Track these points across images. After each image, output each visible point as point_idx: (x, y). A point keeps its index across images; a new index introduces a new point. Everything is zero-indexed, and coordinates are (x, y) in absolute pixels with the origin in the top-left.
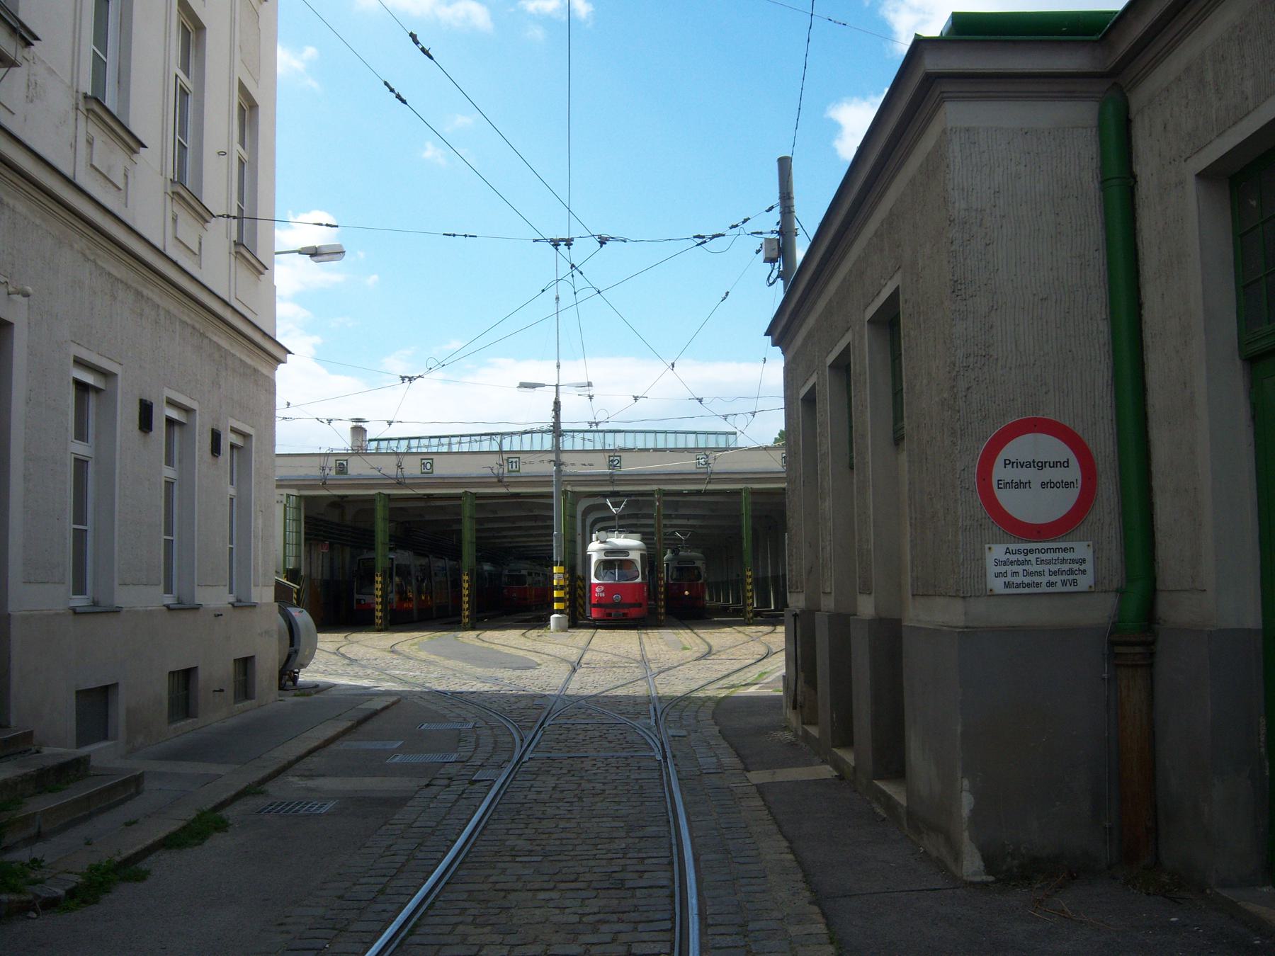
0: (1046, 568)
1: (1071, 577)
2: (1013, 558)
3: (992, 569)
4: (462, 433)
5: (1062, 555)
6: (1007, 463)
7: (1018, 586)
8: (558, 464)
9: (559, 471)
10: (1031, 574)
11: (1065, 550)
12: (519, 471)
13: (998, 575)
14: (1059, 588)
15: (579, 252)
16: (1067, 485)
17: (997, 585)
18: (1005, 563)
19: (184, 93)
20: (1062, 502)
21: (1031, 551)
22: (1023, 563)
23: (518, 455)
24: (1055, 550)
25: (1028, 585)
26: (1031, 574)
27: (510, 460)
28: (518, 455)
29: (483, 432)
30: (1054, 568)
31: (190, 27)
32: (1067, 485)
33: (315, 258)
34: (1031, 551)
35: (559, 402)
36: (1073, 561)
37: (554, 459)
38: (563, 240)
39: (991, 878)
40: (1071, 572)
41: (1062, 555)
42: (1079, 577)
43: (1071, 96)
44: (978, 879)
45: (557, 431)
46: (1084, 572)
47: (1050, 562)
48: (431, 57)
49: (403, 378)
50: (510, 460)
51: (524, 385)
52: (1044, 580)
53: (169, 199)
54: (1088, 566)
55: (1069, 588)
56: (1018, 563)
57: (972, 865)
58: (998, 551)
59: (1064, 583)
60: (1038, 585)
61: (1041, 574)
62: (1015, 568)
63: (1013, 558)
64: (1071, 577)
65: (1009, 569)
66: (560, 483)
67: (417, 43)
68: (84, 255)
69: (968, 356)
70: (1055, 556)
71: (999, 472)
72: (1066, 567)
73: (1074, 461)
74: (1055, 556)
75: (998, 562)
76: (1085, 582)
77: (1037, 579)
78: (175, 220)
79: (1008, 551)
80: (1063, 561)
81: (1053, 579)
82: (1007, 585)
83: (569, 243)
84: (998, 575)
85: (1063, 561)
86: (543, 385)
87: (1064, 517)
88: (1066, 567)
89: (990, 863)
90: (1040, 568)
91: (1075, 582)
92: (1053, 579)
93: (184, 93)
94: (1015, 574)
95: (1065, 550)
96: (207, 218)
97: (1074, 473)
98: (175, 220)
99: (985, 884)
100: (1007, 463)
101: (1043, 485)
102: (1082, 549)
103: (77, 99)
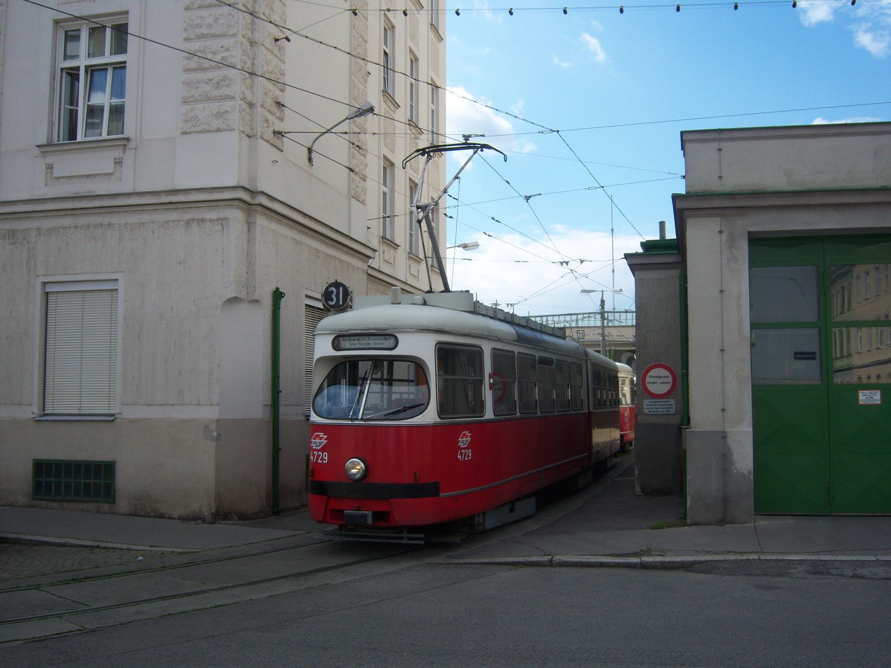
0: (661, 407)
1: (668, 409)
2: (651, 404)
3: (645, 407)
4: (553, 314)
5: (666, 403)
6: (650, 376)
7: (652, 412)
8: (603, 335)
9: (604, 340)
10: (656, 408)
11: (667, 402)
12: (584, 338)
13: (647, 409)
14: (665, 413)
15: (572, 265)
16: (668, 383)
17: (646, 411)
18: (649, 405)
19: (386, 54)
20: (666, 388)
21: (657, 402)
22: (655, 405)
23: (583, 329)
24: (664, 402)
25: (656, 412)
26: (656, 408)
27: (579, 332)
28: (583, 329)
29: (567, 313)
30: (663, 407)
31: (413, 185)
32: (668, 383)
33: (466, 248)
34: (657, 402)
35: (604, 301)
36: (670, 405)
37: (601, 332)
38: (564, 262)
39: (643, 494)
40: (668, 408)
41: (666, 403)
42: (671, 410)
43: (673, 268)
44: (640, 494)
45: (602, 313)
46: (672, 408)
47: (663, 405)
48: (500, 222)
49: (508, 305)
50: (579, 332)
51: (584, 291)
52: (661, 410)
53: (407, 260)
54: (674, 407)
55: (667, 413)
56: (653, 405)
57: (638, 490)
58: (647, 402)
59: (666, 411)
60: (659, 412)
61: (659, 408)
62: (652, 407)
63: (651, 404)
64: (668, 409)
65: (650, 407)
66: (605, 346)
67: (494, 220)
68: (383, 292)
69: (639, 346)
70: (664, 403)
71: (648, 379)
72: (667, 407)
73: (670, 376)
74: (664, 403)
75: (647, 405)
76: (673, 411)
77: (658, 410)
78: (410, 267)
79: (650, 402)
80: (666, 405)
81: (663, 410)
82: (650, 411)
83: (567, 263)
84: (647, 409)
85: (666, 405)
86: (594, 291)
87: (653, 393)
88: (667, 407)
89: (643, 490)
90: (659, 407)
91: (669, 411)
92: (663, 410)
93: (386, 54)
94: (652, 408)
95: (667, 402)
96: (421, 261)
97: (670, 379)
98: (410, 267)
99: (641, 496)
100: (650, 376)
101: (661, 383)
102: (672, 401)
103: (380, 239)
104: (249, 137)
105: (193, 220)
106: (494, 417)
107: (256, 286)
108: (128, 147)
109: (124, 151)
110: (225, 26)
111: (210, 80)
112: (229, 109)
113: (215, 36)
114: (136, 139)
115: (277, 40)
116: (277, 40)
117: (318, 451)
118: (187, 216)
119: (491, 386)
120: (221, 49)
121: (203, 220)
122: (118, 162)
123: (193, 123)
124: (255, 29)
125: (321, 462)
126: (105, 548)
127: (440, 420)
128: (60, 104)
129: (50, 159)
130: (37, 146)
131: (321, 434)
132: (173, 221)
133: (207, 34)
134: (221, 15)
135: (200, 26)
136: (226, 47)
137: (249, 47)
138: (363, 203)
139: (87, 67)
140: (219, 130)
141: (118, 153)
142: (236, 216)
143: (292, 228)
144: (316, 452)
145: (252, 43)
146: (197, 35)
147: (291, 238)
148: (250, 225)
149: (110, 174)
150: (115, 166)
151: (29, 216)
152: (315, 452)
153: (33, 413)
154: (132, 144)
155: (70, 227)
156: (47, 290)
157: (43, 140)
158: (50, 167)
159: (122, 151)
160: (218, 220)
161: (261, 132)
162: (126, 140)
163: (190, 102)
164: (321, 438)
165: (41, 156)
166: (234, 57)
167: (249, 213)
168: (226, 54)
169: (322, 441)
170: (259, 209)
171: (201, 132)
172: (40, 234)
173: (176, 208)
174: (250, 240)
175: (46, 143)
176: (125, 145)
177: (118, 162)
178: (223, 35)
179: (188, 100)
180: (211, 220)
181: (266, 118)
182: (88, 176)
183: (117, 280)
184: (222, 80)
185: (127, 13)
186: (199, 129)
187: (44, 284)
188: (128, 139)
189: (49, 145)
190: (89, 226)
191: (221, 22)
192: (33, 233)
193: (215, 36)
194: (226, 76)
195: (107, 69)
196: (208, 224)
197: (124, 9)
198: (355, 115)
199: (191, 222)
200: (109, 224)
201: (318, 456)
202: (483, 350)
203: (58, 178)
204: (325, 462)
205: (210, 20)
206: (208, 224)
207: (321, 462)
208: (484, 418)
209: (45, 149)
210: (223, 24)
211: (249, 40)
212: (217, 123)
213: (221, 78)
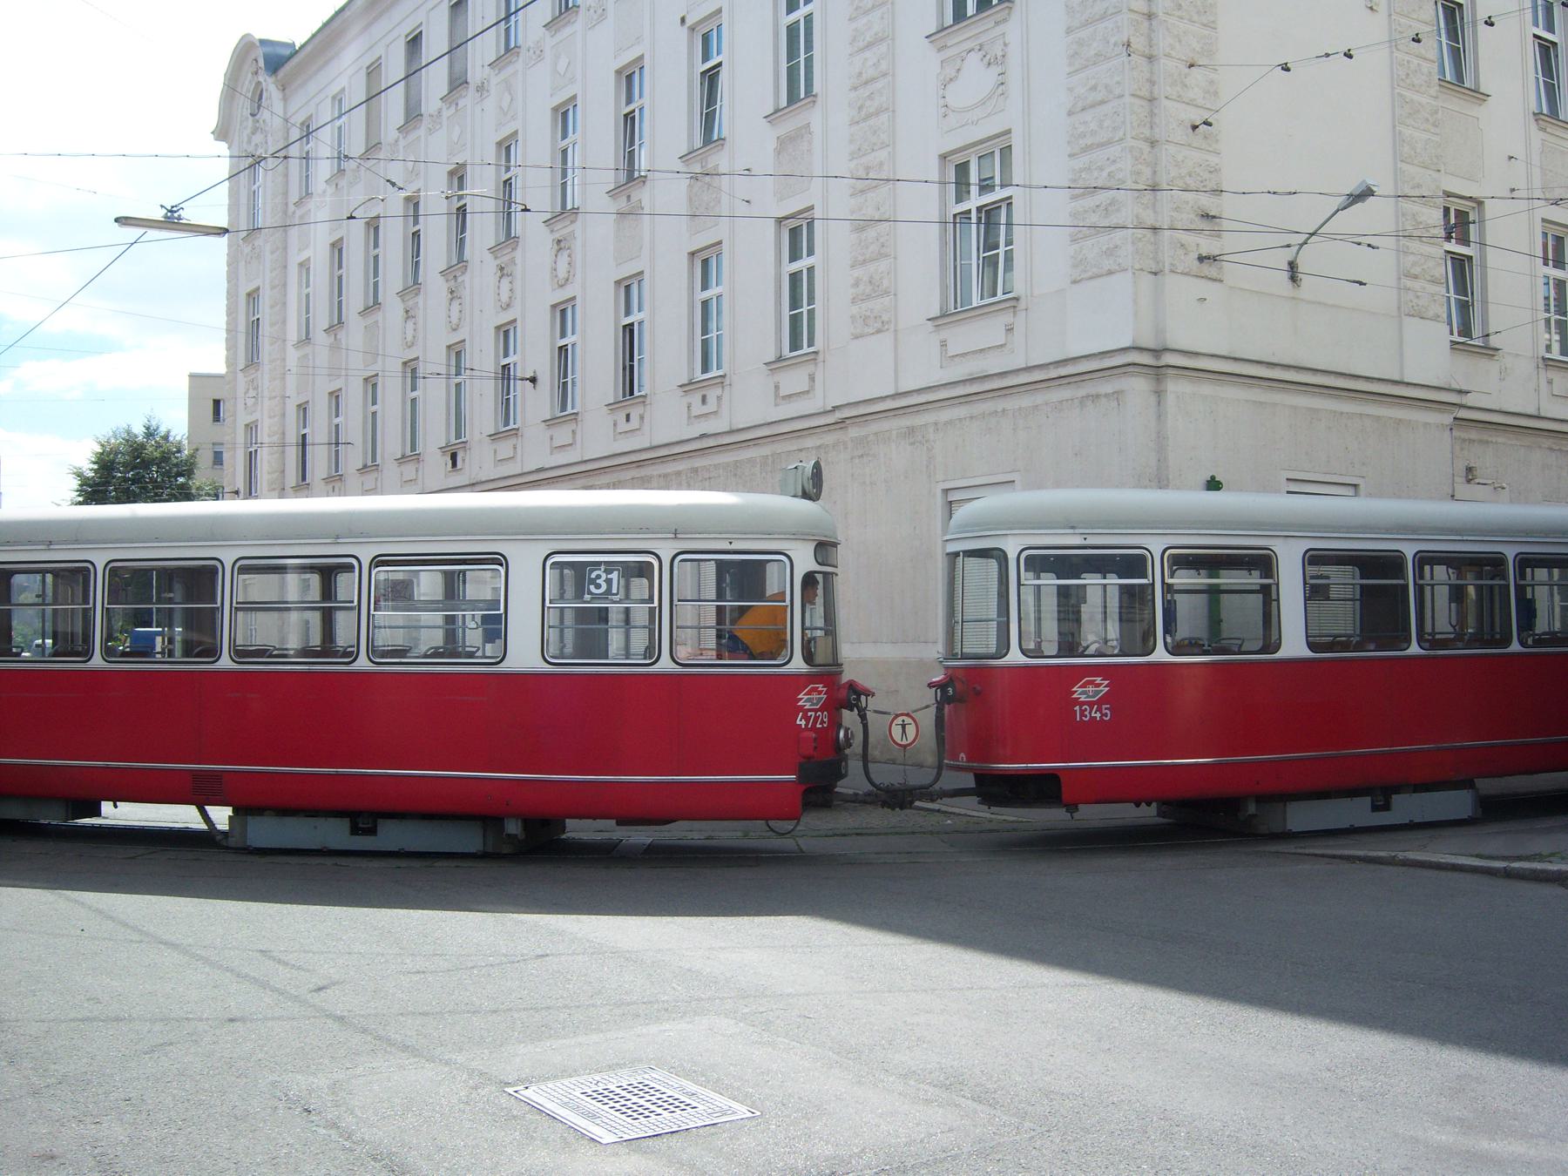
104: (1155, 274)
105: (1088, 396)
106: (1307, 653)
107: (1170, 477)
108: (1017, 309)
109: (1015, 313)
110: (1110, 129)
111: (1097, 206)
112: (1119, 243)
113: (1101, 145)
114: (1027, 296)
115: (1195, 127)
116: (1195, 127)
117: (815, 711)
118: (1082, 392)
119: (1559, 593)
120: (1108, 162)
121: (1098, 396)
122: (812, 378)
123: (1083, 267)
124: (1155, 123)
125: (820, 726)
126: (946, 812)
127: (1522, 648)
128: (955, 260)
129: (945, 334)
130: (929, 320)
131: (1098, 680)
132: (1067, 400)
133: (1092, 144)
134: (1106, 115)
135: (1082, 135)
136: (1112, 158)
137: (1149, 149)
138: (1439, 319)
139: (979, 209)
140: (1110, 273)
141: (1007, 318)
142: (1137, 387)
143: (1251, 386)
144: (813, 713)
145: (1153, 143)
146: (1082, 148)
147: (1247, 401)
148: (1159, 394)
149: (1002, 346)
150: (1006, 334)
151: (925, 408)
152: (809, 714)
153: (938, 652)
154: (1022, 305)
155: (965, 418)
156: (949, 500)
157: (936, 312)
158: (944, 344)
159: (1012, 315)
160: (1113, 393)
161: (1171, 264)
162: (1015, 301)
163: (1078, 239)
164: (820, 693)
165: (935, 331)
166: (1121, 170)
167: (1158, 379)
168: (1113, 168)
169: (1101, 688)
170: (1170, 371)
171: (1091, 278)
172: (938, 430)
173: (1069, 383)
174: (1160, 416)
175: (939, 315)
176: (1014, 307)
177: (1010, 330)
178: (1109, 143)
179: (1076, 237)
180: (1106, 395)
181: (1180, 242)
182: (981, 351)
183: (1014, 481)
184: (1110, 204)
185: (1008, 132)
186: (1090, 274)
187: (946, 491)
188: (1017, 299)
189: (943, 316)
190: (983, 415)
191: (1106, 124)
192: (931, 430)
193: (1101, 145)
194: (1114, 198)
195: (1000, 206)
196: (1104, 400)
197: (1007, 128)
198: (1347, 202)
199: (674, 477)
200: (1004, 410)
201: (816, 718)
202: (1400, 551)
203: (790, 396)
204: (825, 725)
205: (1093, 126)
206: (1104, 400)
207: (820, 726)
208: (1277, 655)
209: (940, 322)
210: (1108, 127)
211: (1146, 140)
212: (1108, 264)
213: (1108, 202)
